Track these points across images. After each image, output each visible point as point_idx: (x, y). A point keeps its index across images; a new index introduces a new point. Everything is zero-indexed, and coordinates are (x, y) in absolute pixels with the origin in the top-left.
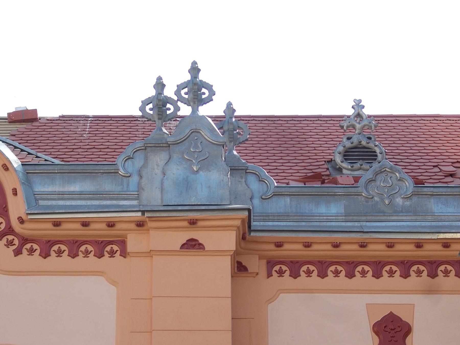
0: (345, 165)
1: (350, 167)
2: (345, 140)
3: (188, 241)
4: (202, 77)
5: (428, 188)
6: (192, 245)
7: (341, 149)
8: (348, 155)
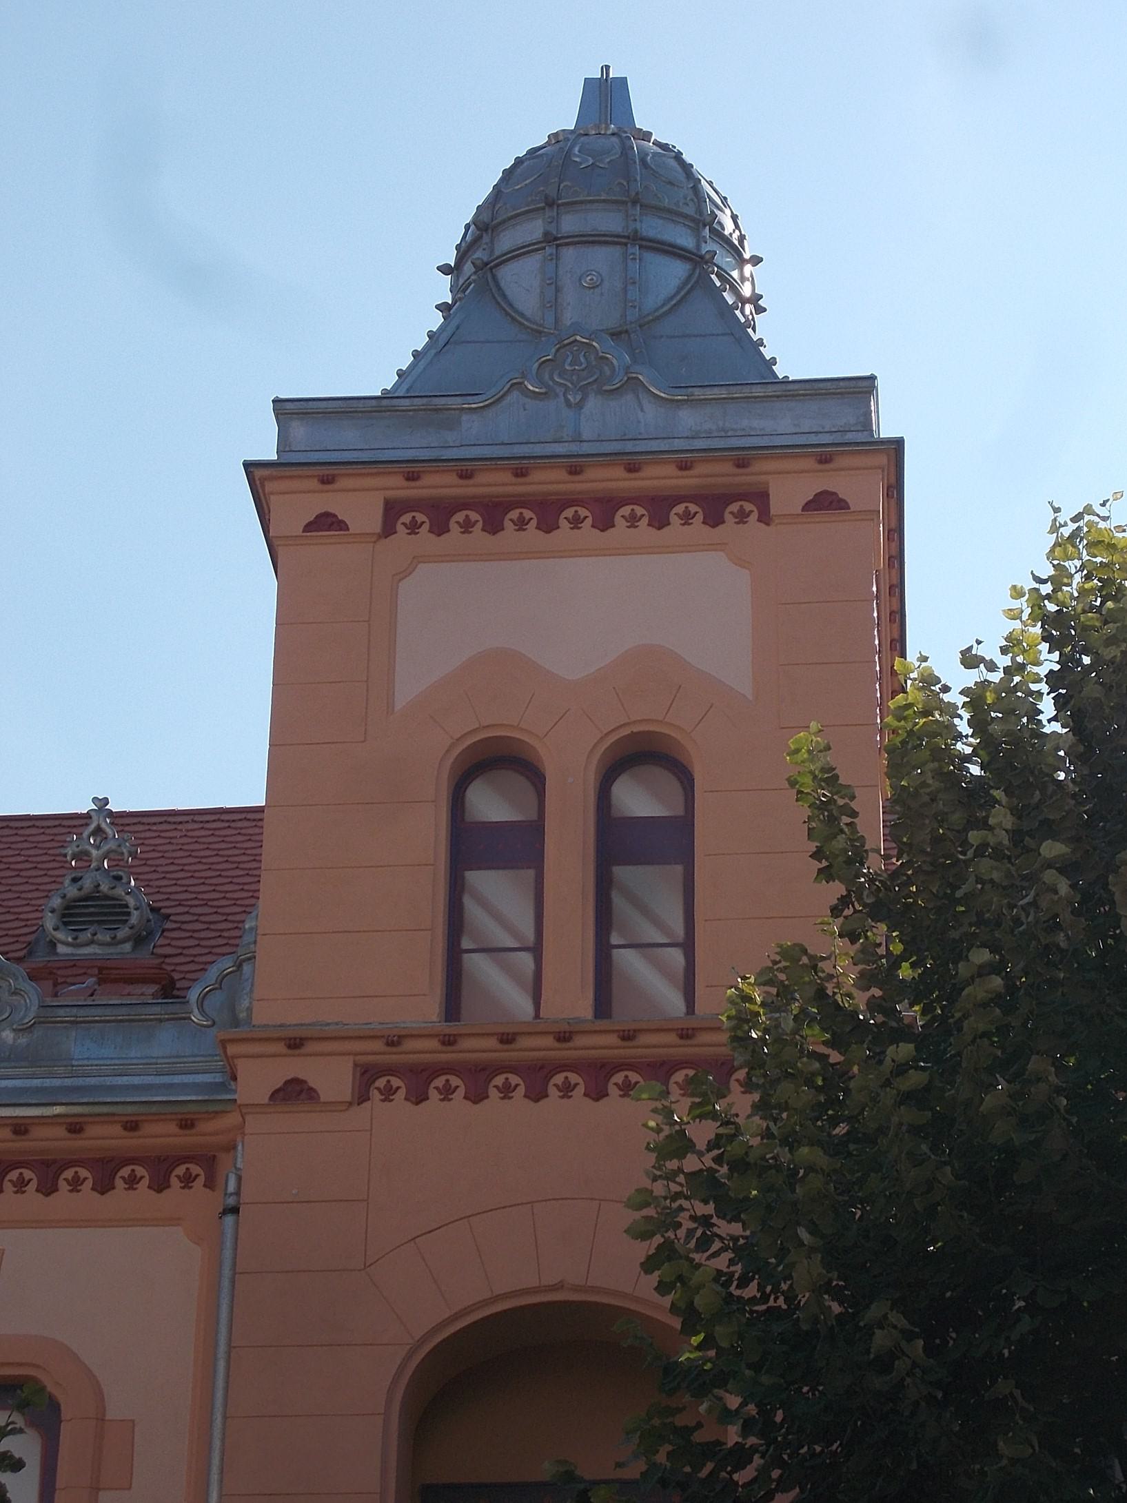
0: (60, 935)
1: (70, 939)
2: (67, 882)
3: (288, 1083)
5: (68, 1010)
7: (56, 902)
8: (70, 915)
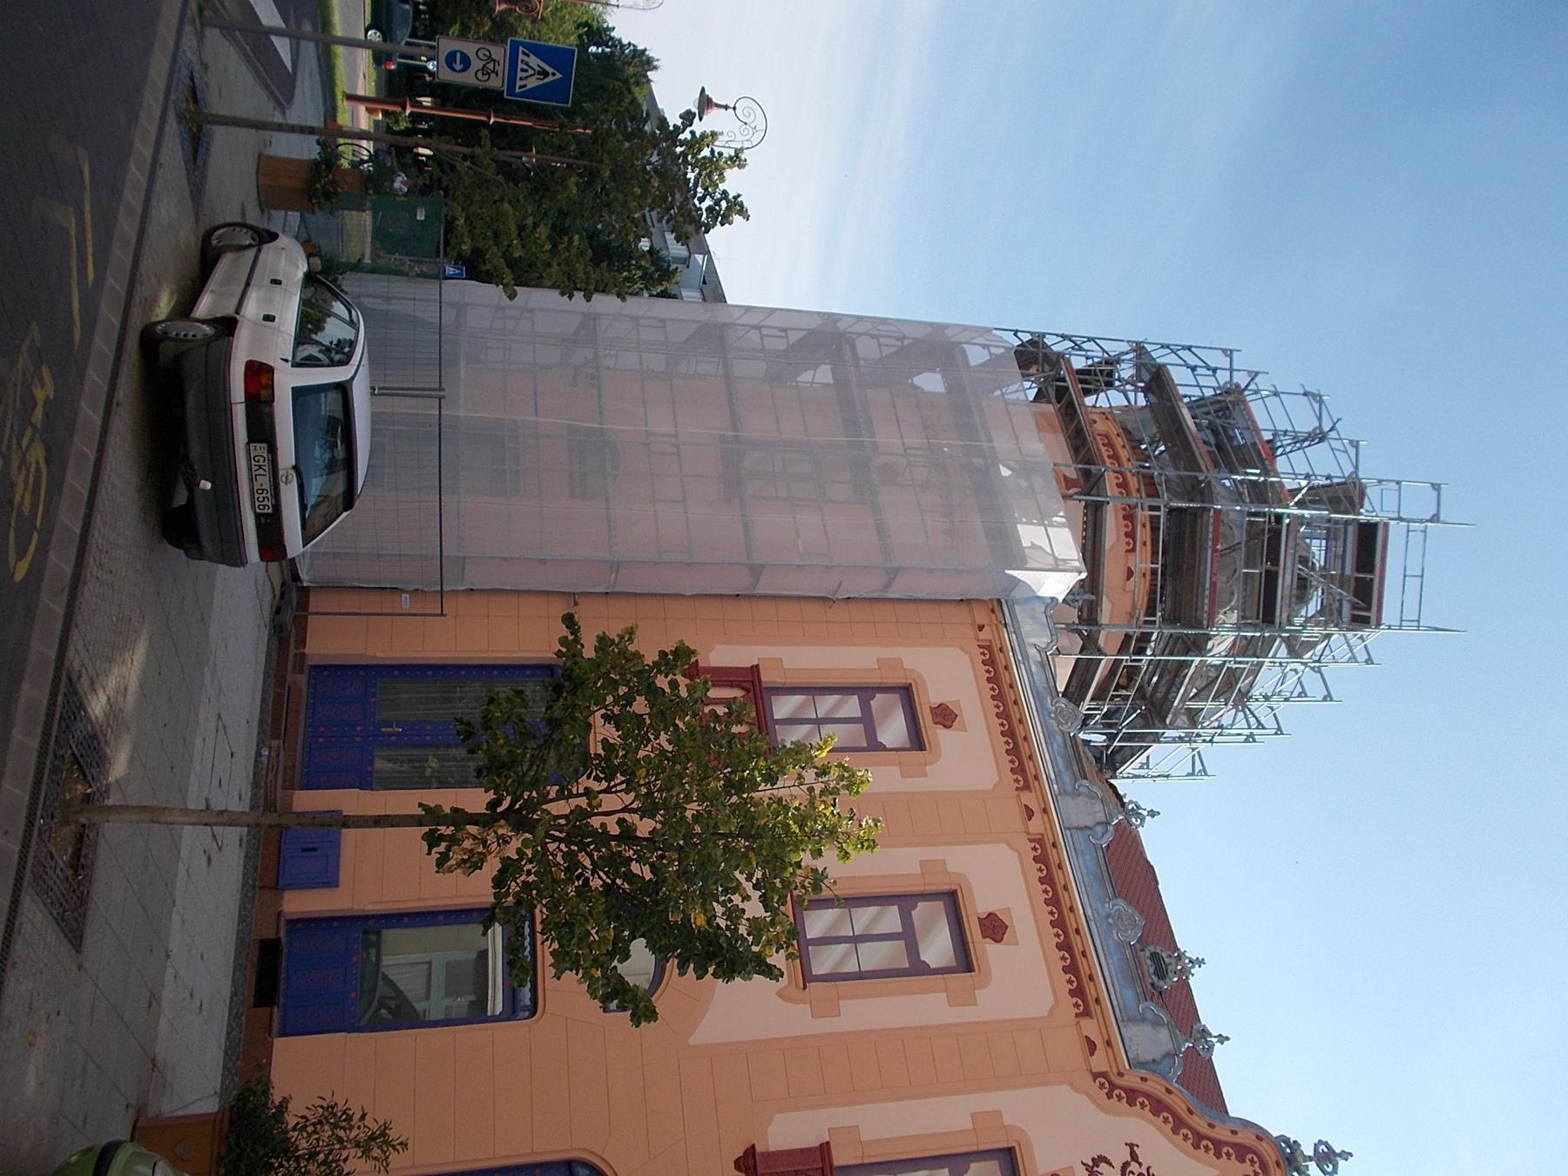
4: (1341, 1162)
6: (1092, 1046)
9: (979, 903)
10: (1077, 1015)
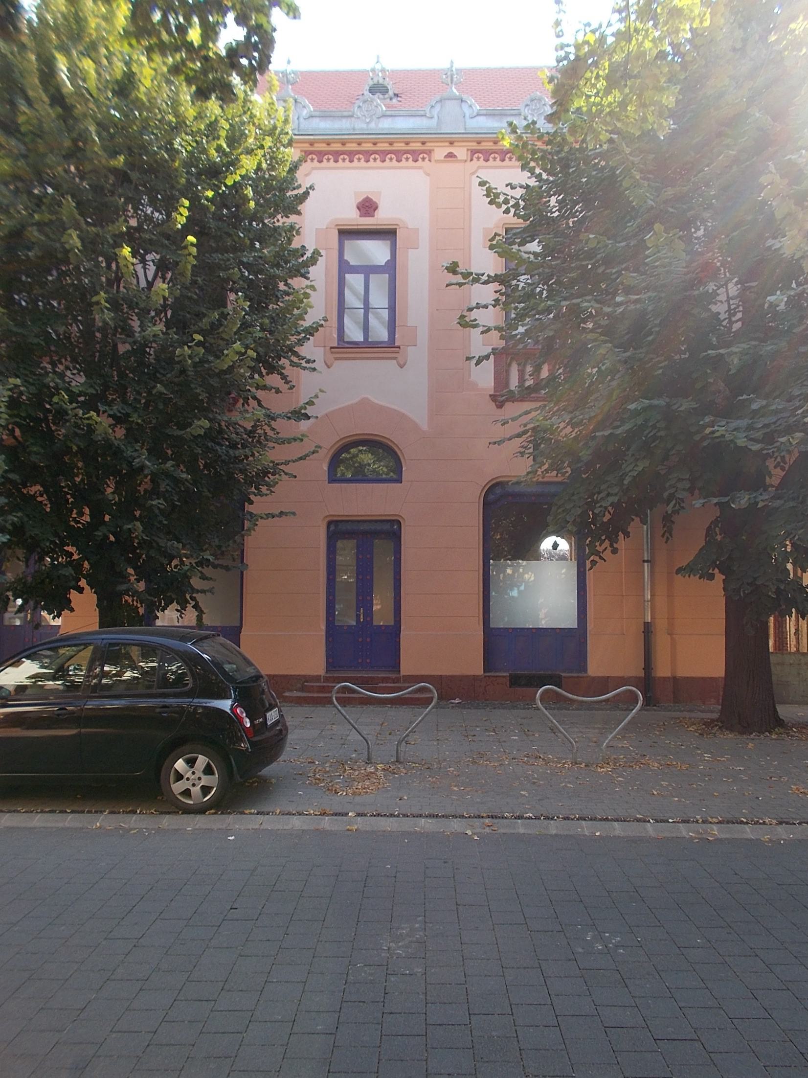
9: (351, 217)
10: (430, 161)
